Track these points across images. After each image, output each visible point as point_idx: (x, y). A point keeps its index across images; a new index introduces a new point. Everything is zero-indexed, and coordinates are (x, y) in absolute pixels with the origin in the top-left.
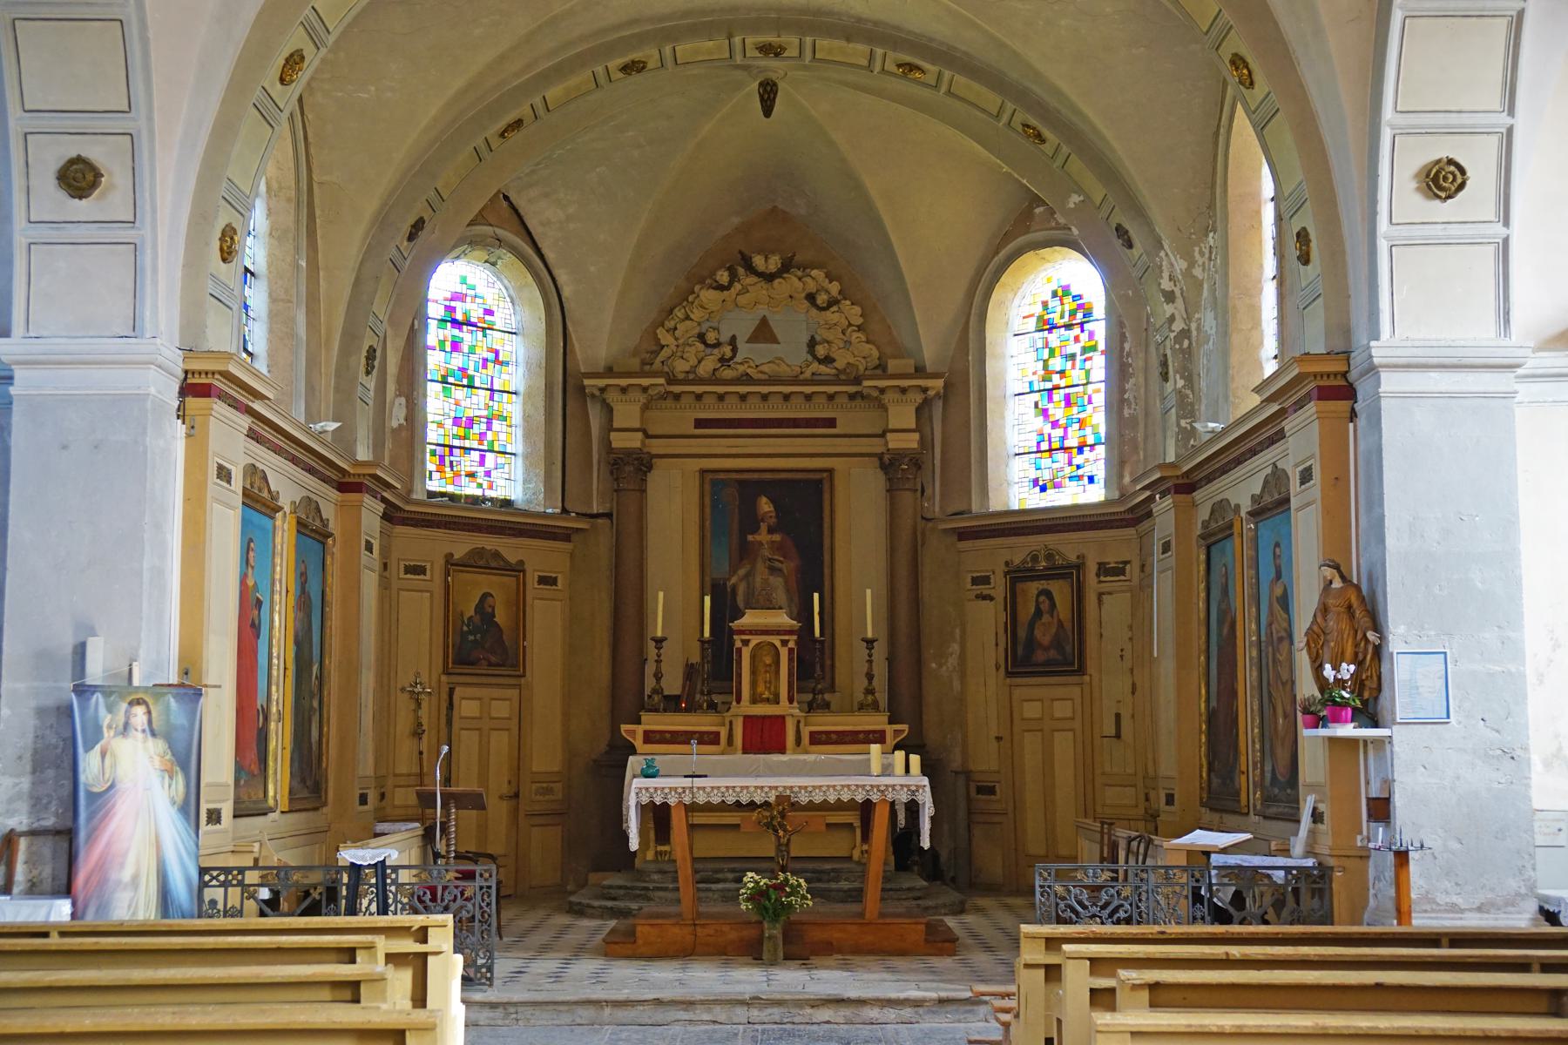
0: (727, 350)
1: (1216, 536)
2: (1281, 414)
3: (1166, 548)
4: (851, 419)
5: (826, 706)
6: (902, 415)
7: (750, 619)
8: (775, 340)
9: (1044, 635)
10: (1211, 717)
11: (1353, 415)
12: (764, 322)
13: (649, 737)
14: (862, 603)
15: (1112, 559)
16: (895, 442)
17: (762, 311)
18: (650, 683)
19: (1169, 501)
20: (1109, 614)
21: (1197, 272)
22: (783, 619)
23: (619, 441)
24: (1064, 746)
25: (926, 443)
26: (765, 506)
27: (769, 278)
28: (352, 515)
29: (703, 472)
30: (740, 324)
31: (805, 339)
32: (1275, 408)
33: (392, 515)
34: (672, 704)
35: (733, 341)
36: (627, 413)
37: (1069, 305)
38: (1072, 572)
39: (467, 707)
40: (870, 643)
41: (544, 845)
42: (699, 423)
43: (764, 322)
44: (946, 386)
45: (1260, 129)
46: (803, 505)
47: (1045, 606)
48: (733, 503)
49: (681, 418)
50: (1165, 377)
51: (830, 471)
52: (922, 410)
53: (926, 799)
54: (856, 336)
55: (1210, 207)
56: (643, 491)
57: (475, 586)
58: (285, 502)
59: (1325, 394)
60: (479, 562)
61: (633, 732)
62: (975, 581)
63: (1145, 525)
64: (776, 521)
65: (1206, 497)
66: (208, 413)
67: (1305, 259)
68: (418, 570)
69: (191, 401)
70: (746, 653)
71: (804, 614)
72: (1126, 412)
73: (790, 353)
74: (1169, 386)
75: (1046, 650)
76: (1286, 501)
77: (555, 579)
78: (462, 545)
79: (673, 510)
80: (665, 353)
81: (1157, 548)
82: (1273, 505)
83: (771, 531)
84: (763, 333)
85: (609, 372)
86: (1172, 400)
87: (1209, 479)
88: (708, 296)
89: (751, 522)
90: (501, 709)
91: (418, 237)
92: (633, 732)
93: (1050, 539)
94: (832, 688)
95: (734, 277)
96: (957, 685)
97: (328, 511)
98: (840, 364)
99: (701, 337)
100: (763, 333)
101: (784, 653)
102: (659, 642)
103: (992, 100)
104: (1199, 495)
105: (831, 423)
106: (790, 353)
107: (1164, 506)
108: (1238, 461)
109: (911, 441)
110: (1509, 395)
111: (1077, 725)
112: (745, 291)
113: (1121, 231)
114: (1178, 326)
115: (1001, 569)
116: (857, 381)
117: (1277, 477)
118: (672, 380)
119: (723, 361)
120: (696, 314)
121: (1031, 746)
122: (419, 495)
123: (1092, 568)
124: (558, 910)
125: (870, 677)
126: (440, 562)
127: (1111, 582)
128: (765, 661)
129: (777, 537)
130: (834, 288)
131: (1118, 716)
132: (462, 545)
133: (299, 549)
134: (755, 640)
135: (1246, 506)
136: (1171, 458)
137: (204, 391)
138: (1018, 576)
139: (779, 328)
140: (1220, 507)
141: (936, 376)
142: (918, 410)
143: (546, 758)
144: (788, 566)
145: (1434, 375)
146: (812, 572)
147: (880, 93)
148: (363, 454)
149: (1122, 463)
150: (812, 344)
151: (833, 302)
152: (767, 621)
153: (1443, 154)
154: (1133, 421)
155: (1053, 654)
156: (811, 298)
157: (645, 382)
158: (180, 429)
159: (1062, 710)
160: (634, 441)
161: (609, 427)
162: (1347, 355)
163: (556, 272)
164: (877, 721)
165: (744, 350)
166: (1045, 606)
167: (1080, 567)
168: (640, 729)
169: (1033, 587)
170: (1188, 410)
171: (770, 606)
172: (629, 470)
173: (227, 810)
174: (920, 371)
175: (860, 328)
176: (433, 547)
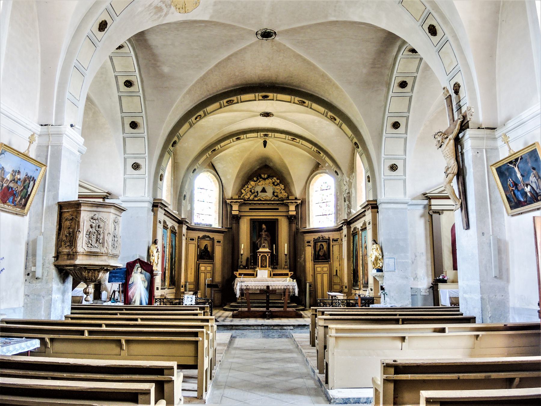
0: (256, 194)
1: (355, 234)
2: (365, 211)
3: (345, 236)
4: (282, 209)
5: (276, 268)
6: (292, 208)
7: (260, 250)
8: (266, 192)
9: (321, 254)
10: (354, 270)
11: (378, 212)
12: (264, 188)
13: (240, 274)
14: (284, 248)
15: (335, 238)
16: (291, 213)
17: (263, 186)
18: (240, 263)
19: (346, 226)
20: (335, 249)
21: (351, 181)
22: (267, 250)
23: (233, 213)
24: (326, 277)
25: (297, 213)
26: (264, 226)
27: (265, 179)
28: (180, 228)
29: (251, 219)
30: (259, 189)
31: (272, 191)
32: (364, 210)
33: (189, 229)
34: (244, 268)
35: (257, 192)
36: (235, 207)
37: (326, 185)
38: (328, 241)
39: (202, 268)
40: (286, 255)
41: (217, 297)
42: (250, 209)
43: (264, 188)
44: (302, 202)
45: (361, 156)
46: (272, 226)
47: (321, 247)
48: (256, 225)
49: (247, 208)
50: (345, 201)
51: (277, 219)
52: (297, 207)
53: (296, 287)
54: (283, 191)
55: (352, 168)
56: (239, 223)
57: (205, 243)
58: (169, 227)
59: (373, 208)
60: (204, 237)
61: (237, 273)
62: (307, 242)
63: (341, 231)
64: (265, 230)
65: (352, 226)
66: (157, 211)
67: (369, 181)
68: (192, 240)
69: (155, 208)
70: (260, 257)
71: (271, 249)
72: (338, 208)
73: (269, 195)
74: (346, 203)
75: (323, 256)
76: (366, 228)
77: (474, 318)
78: (201, 234)
79: (245, 227)
80: (243, 195)
81: (344, 236)
82: (364, 229)
83: (265, 231)
84: (264, 190)
85: (232, 199)
86: (346, 206)
87: (353, 222)
88: (252, 183)
89: (261, 229)
90: (209, 269)
91: (192, 169)
92: (237, 273)
93: (323, 234)
94: (277, 265)
95: (258, 179)
96: (303, 264)
97: (176, 228)
98: (280, 197)
99: (251, 191)
100: (264, 190)
101: (268, 257)
102: (242, 255)
103: (310, 146)
104: (351, 225)
105: (278, 209)
106: (269, 195)
107: (345, 228)
108: (358, 219)
109: (294, 213)
110: (406, 209)
111: (328, 272)
112: (260, 182)
113: (336, 172)
114: (347, 191)
115: (312, 240)
116: (283, 201)
117: (365, 224)
118: (245, 200)
119: (255, 196)
120: (250, 187)
121: (319, 277)
122: (193, 224)
123: (331, 240)
124: (222, 310)
125: (286, 262)
126: (197, 238)
127: (335, 243)
128: (264, 258)
129: (266, 233)
130: (278, 181)
131: (337, 271)
132: (201, 234)
133: (170, 235)
134: (262, 254)
135: (360, 228)
136: (346, 218)
137: (157, 206)
138: (316, 241)
139: (267, 189)
140: (355, 229)
141: (299, 200)
142: (296, 207)
143: (218, 279)
144: (269, 239)
145: (392, 205)
146: (273, 240)
147: (287, 143)
148: (183, 217)
149: (337, 218)
150: (274, 193)
151: (278, 184)
152: (264, 250)
153: (393, 163)
154: (340, 210)
155: (323, 258)
156: (273, 183)
157: (239, 201)
158: (152, 213)
159: (325, 269)
160: (237, 213)
161: (231, 210)
162: (376, 201)
163: (222, 178)
164: (287, 271)
165: (260, 194)
166: (321, 247)
167: (329, 239)
168: (238, 273)
169: (319, 244)
170: (349, 207)
171: (264, 247)
172: (236, 219)
173: (160, 288)
174: (296, 199)
175: (284, 190)
176: (195, 235)
